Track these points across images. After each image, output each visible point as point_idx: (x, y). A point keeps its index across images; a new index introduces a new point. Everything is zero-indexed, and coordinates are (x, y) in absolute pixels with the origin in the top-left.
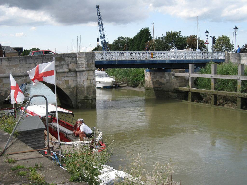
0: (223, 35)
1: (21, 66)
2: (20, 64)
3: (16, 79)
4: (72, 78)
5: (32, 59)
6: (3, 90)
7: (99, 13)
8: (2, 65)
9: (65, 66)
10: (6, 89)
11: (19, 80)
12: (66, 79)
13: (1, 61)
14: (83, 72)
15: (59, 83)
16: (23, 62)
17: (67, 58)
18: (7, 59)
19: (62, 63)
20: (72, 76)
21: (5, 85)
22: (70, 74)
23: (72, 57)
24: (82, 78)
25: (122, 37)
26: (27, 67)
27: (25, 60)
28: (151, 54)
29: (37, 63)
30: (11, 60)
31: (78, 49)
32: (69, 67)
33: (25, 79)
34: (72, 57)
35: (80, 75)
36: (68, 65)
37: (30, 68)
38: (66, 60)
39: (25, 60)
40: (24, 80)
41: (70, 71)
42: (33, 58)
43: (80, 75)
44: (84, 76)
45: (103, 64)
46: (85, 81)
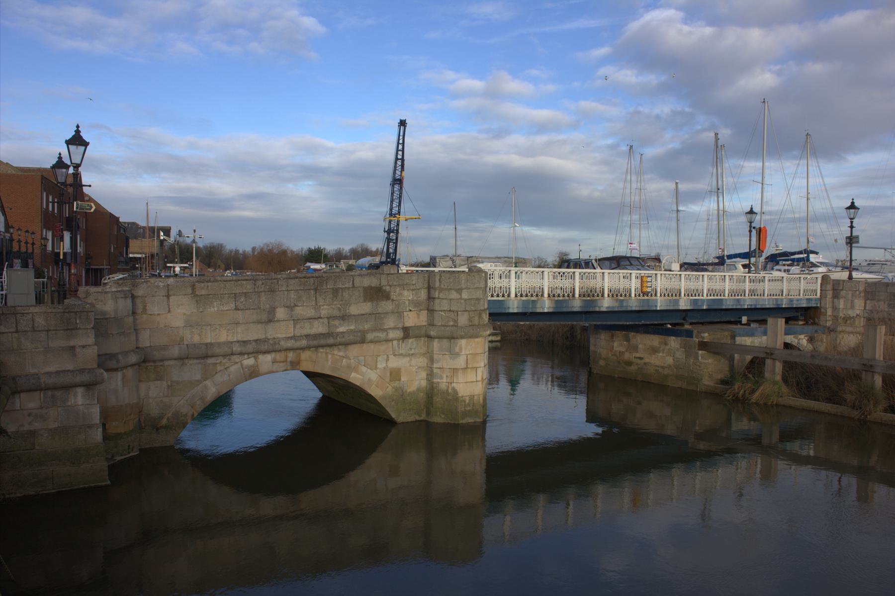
8: (169, 311)
9: (390, 322)
12: (394, 363)
15: (369, 380)
19: (387, 306)
20: (412, 352)
28: (642, 281)
33: (253, 366)
38: (393, 296)
46: (460, 372)
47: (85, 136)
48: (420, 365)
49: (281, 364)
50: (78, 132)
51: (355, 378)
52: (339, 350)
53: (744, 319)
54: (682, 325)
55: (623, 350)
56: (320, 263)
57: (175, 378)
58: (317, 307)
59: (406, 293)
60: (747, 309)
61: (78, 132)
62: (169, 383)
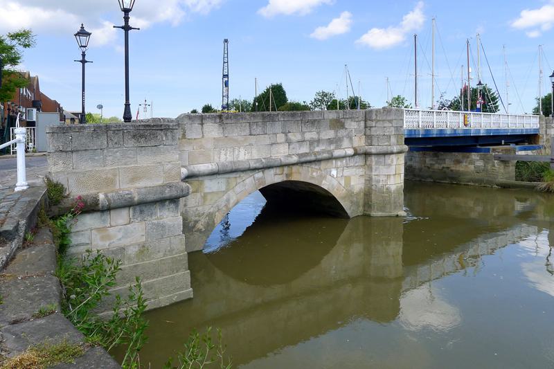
0: (110, 213)
1: (252, 139)
2: (250, 135)
3: (240, 177)
4: (357, 170)
5: (280, 123)
6: (203, 214)
7: (227, 75)
8: (203, 136)
9: (346, 143)
10: (211, 210)
11: (248, 181)
13: (202, 124)
14: (386, 156)
16: (259, 130)
17: (349, 121)
18: (218, 120)
19: (342, 133)
20: (357, 165)
21: (209, 197)
22: (352, 162)
23: (357, 120)
24: (383, 170)
25: (62, 185)
26: (268, 142)
27: (264, 123)
29: (289, 132)
30: (229, 121)
31: (462, 75)
32: (352, 144)
33: (261, 178)
34: (357, 120)
35: (377, 163)
36: (351, 139)
37: (274, 145)
39: (264, 123)
40: (259, 179)
41: (356, 154)
42: (282, 119)
43: (377, 163)
44: (390, 165)
45: (431, 136)
46: (392, 177)
47: (87, 29)
48: (361, 173)
49: (280, 176)
50: (82, 28)
51: (325, 185)
52: (316, 165)
53: (503, 142)
54: (476, 145)
55: (434, 163)
56: (28, 177)
57: (207, 190)
58: (303, 133)
59: (353, 123)
60: (510, 135)
61: (82, 28)
62: (203, 194)
